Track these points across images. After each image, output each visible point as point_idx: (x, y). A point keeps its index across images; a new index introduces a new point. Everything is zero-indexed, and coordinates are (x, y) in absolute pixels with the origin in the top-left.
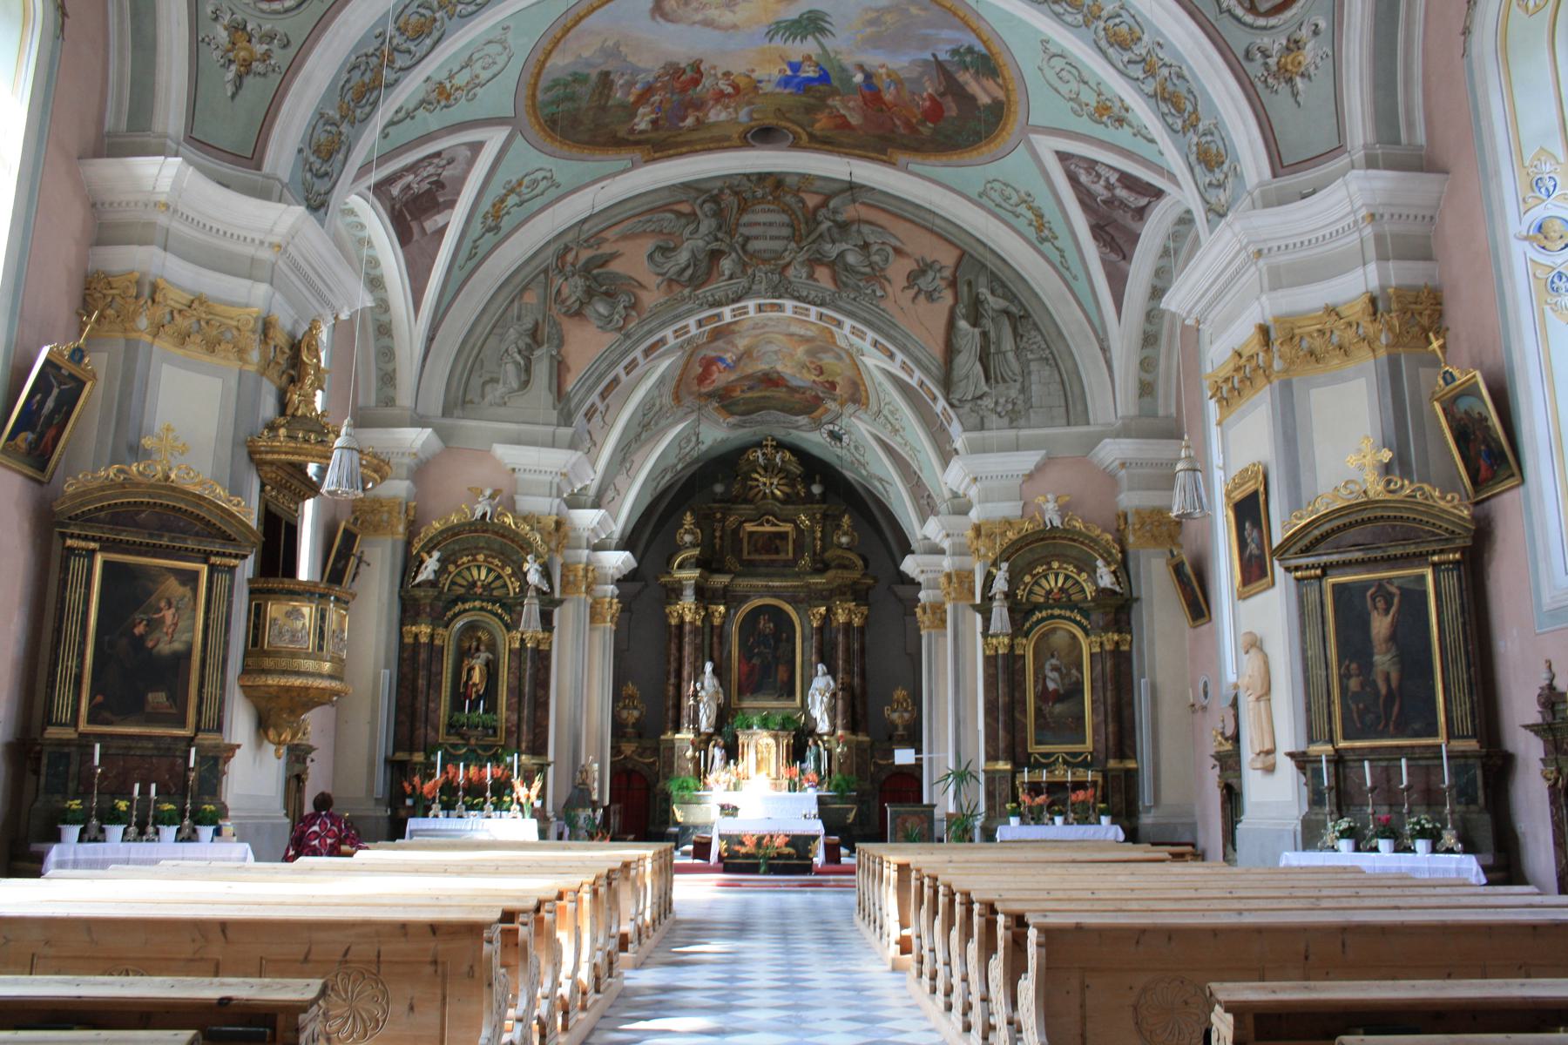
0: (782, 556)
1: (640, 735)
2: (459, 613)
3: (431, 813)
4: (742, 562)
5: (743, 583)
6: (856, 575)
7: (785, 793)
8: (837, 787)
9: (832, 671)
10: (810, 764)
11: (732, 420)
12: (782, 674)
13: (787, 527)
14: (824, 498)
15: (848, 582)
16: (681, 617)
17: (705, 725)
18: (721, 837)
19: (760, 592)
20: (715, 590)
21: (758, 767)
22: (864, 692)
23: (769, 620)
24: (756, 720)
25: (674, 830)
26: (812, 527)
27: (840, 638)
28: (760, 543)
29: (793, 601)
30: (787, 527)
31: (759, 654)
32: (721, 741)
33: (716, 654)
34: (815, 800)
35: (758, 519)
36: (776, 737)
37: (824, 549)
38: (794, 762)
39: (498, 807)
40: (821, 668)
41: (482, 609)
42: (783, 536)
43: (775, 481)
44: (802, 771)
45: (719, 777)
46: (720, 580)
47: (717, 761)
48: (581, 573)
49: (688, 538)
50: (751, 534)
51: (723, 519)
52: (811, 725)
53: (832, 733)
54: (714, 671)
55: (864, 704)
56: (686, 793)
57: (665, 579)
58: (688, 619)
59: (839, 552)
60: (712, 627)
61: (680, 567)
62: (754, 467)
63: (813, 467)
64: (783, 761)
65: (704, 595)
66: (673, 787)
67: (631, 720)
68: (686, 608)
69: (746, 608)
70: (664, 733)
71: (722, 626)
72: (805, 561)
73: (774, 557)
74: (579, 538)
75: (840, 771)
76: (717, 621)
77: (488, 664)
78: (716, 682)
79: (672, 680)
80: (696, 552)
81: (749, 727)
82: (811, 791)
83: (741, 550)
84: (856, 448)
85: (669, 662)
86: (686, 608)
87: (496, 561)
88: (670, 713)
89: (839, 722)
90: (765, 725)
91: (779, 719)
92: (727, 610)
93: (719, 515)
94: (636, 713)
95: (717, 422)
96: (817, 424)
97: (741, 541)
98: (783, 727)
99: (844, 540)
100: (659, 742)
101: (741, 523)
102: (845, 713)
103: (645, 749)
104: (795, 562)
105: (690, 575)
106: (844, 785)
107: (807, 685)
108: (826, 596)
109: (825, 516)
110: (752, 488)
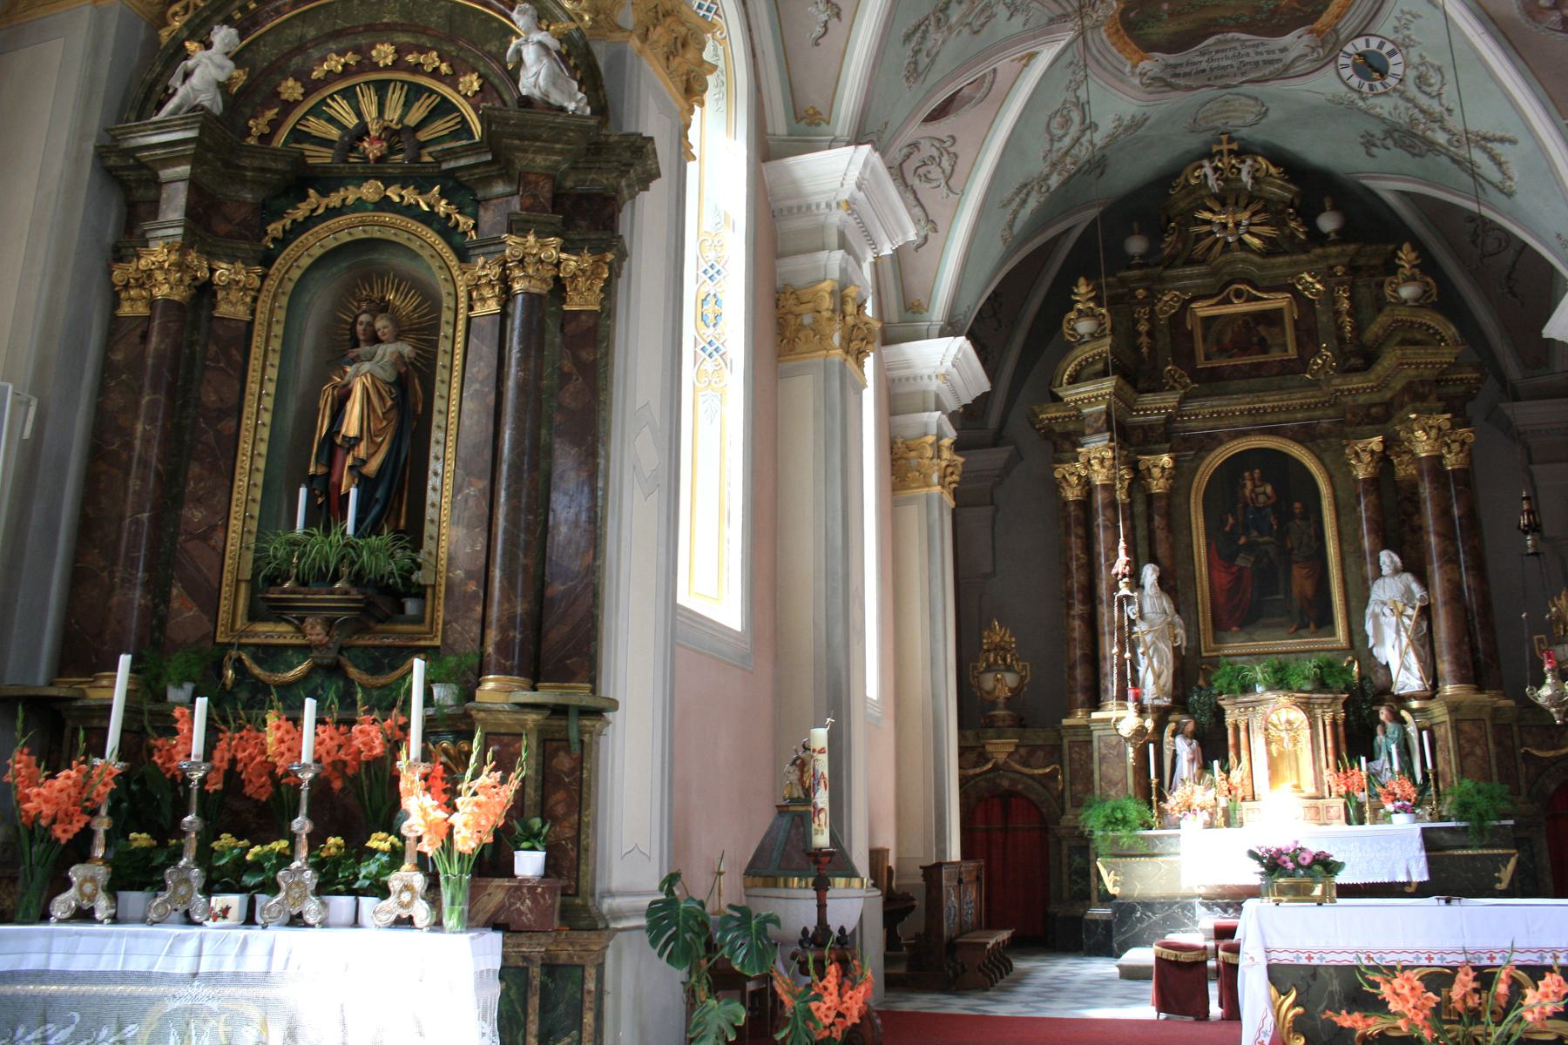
0: (1275, 355)
1: (1020, 723)
2: (311, 221)
3: (63, 904)
4: (1196, 375)
5: (1203, 412)
6: (1446, 355)
7: (1340, 826)
8: (1464, 809)
9: (1414, 566)
10: (1388, 762)
11: (1152, 64)
12: (1301, 582)
13: (1279, 301)
14: (1344, 235)
15: (1428, 374)
16: (1087, 483)
17: (1153, 679)
18: (1279, 976)
19: (1239, 427)
20: (1147, 429)
21: (1273, 765)
22: (1486, 603)
23: (1264, 479)
24: (1259, 672)
25: (1100, 912)
26: (1330, 291)
27: (1426, 490)
28: (1227, 338)
29: (1305, 436)
30: (1279, 301)
31: (1250, 547)
32: (1190, 727)
33: (1162, 550)
34: (1417, 842)
35: (1219, 292)
36: (1307, 707)
37: (1358, 329)
38: (1353, 756)
39: (333, 879)
40: (1387, 559)
41: (385, 204)
42: (1272, 318)
43: (1244, 217)
44: (1373, 776)
45: (1191, 792)
46: (1157, 405)
47: (1185, 768)
48: (827, 303)
49: (1085, 326)
50: (1208, 321)
51: (1152, 298)
52: (1379, 679)
53: (1433, 691)
54: (1161, 581)
55: (1488, 626)
56: (1122, 832)
57: (1051, 413)
58: (1099, 479)
59: (1403, 314)
60: (1150, 498)
61: (1075, 379)
62: (1199, 197)
63: (1313, 185)
64: (1327, 756)
65: (1131, 439)
66: (1093, 821)
67: (1003, 693)
68: (1097, 459)
69: (1217, 457)
70: (1068, 714)
71: (1170, 494)
72: (1325, 356)
73: (1261, 358)
74: (821, 229)
75: (1462, 772)
76: (1158, 485)
77: (401, 384)
78: (1166, 603)
79: (1078, 609)
80: (1105, 344)
81: (1247, 689)
82: (1401, 820)
83: (1192, 354)
84: (1421, 81)
85: (1068, 572)
86: (1097, 459)
87: (431, 60)
88: (1079, 673)
89: (1445, 667)
90: (1280, 682)
91: (1310, 667)
92: (1175, 459)
93: (1141, 293)
94: (1011, 679)
96: (1329, 47)
97: (1190, 335)
98: (1322, 685)
99: (1406, 292)
100: (1059, 732)
101: (1185, 305)
102: (1456, 645)
103: (1033, 749)
104: (1302, 364)
105: (1093, 395)
106: (1482, 803)
107: (1358, 600)
108: (1381, 416)
109: (1353, 269)
110: (1199, 238)
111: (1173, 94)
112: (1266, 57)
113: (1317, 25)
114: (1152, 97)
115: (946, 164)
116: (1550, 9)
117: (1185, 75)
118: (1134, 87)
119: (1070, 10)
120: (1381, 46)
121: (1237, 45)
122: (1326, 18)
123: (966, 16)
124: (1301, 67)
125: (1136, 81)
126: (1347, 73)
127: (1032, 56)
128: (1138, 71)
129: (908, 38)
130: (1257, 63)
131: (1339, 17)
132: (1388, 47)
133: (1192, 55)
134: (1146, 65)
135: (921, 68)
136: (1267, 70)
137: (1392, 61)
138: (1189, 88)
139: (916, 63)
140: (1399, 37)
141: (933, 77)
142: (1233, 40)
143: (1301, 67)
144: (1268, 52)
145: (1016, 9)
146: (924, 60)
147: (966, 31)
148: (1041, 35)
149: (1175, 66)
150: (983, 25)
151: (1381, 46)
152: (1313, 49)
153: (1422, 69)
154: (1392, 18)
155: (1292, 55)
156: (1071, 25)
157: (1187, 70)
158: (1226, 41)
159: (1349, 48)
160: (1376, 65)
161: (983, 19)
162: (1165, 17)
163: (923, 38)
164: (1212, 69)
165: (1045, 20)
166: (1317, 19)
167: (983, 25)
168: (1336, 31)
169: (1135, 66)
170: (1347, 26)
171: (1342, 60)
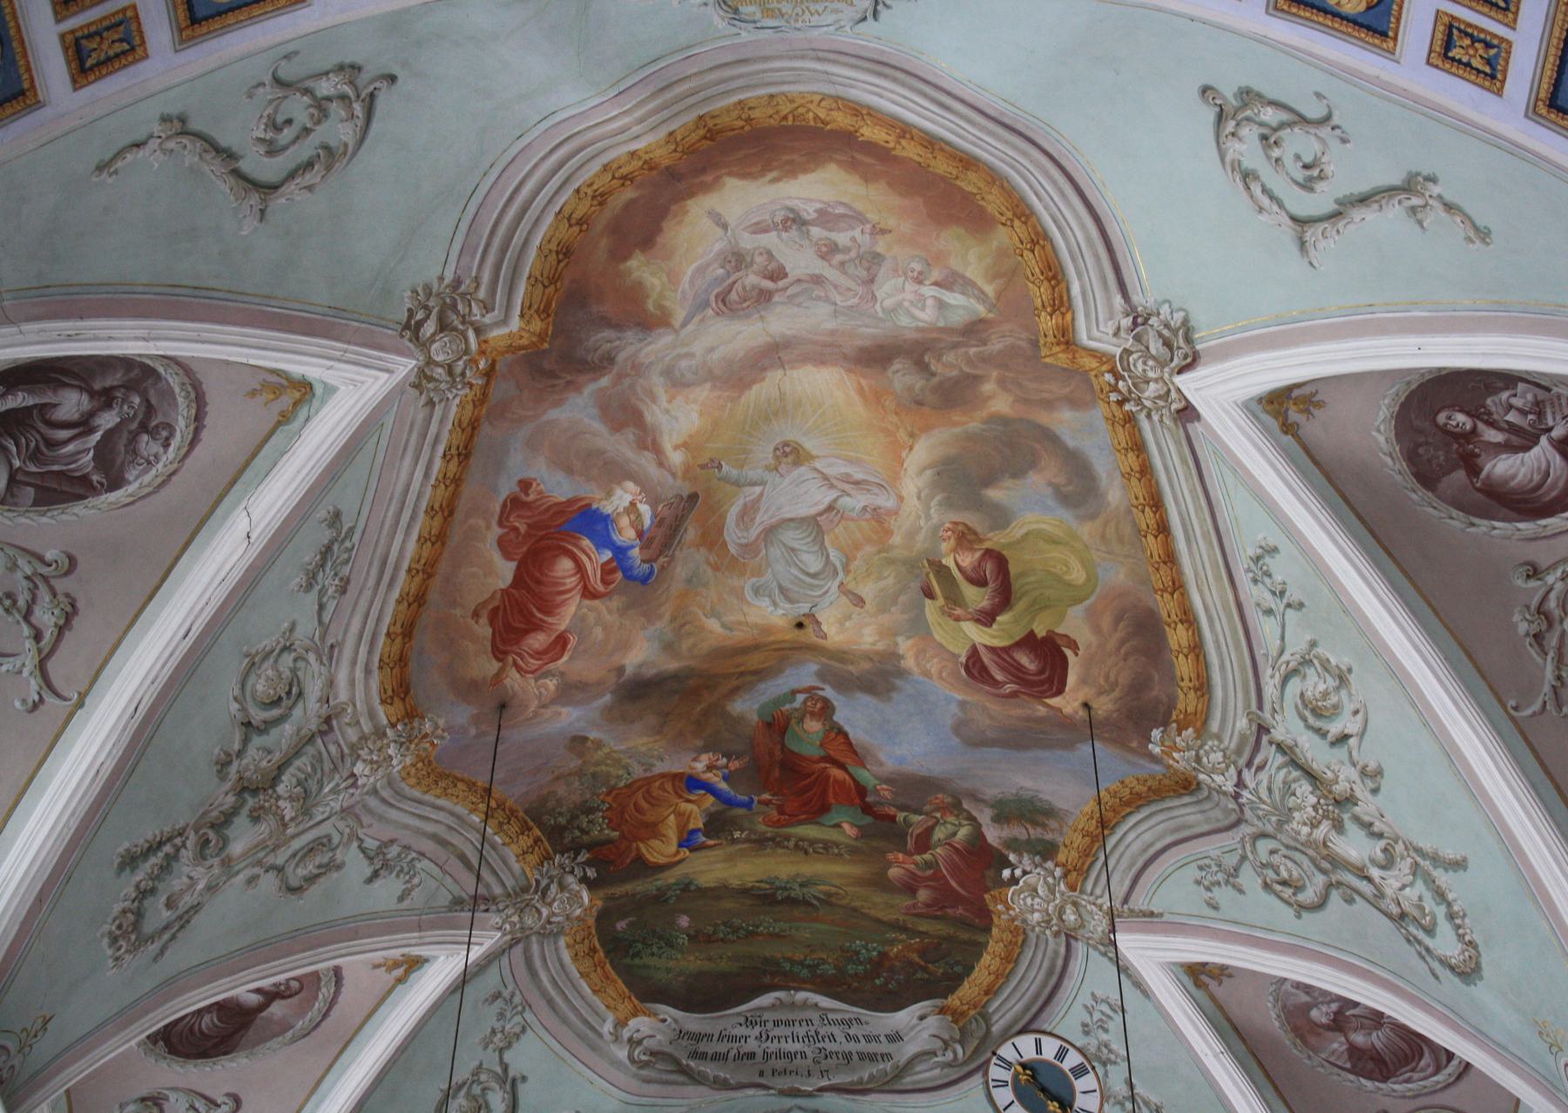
11: (655, 1025)
95: (589, 1038)
111: (691, 1090)
112: (863, 1046)
113: (953, 1001)
114: (653, 1088)
115: (46, 617)
116: (1328, 1028)
117: (716, 1057)
118: (616, 1063)
119: (498, 890)
120: (1061, 1054)
121: (815, 1016)
122: (968, 990)
123: (261, 846)
124: (925, 1073)
125: (622, 1054)
126: (1004, 1096)
127: (414, 964)
128: (626, 1033)
129: (130, 861)
130: (848, 1056)
131: (991, 991)
132: (1073, 1059)
133: (728, 1021)
134: (641, 1025)
135: (149, 927)
136: (866, 1072)
137: (1080, 1084)
138: (724, 1085)
139: (139, 914)
140: (1091, 1043)
141: (184, 954)
142: (805, 1005)
143: (925, 1073)
144: (868, 1039)
145: (386, 865)
146: (158, 914)
147: (269, 882)
148: (433, 926)
149: (698, 1037)
150: (312, 879)
151: (1061, 1054)
152: (946, 1045)
153: (1233, 757)
154: (1078, 1007)
155: (909, 1049)
156: (496, 919)
157: (722, 1048)
158: (793, 1006)
159: (1006, 1051)
160: (1053, 1088)
161: (310, 868)
162: (683, 940)
163: (166, 868)
164: (767, 1056)
165: (444, 899)
166: (951, 990)
167: (312, 879)
168: (986, 1017)
169: (621, 1024)
170: (1005, 1010)
171: (996, 1072)
